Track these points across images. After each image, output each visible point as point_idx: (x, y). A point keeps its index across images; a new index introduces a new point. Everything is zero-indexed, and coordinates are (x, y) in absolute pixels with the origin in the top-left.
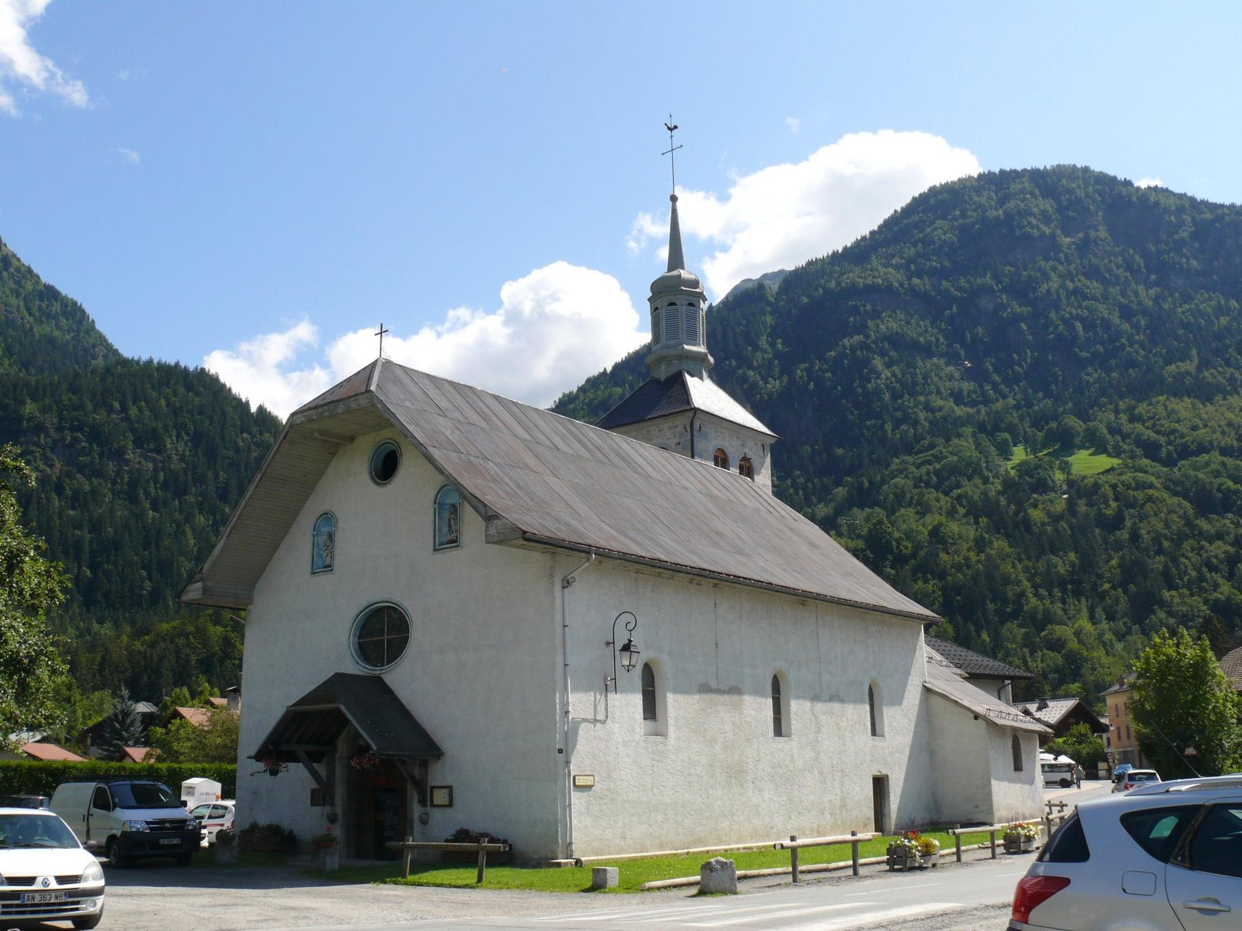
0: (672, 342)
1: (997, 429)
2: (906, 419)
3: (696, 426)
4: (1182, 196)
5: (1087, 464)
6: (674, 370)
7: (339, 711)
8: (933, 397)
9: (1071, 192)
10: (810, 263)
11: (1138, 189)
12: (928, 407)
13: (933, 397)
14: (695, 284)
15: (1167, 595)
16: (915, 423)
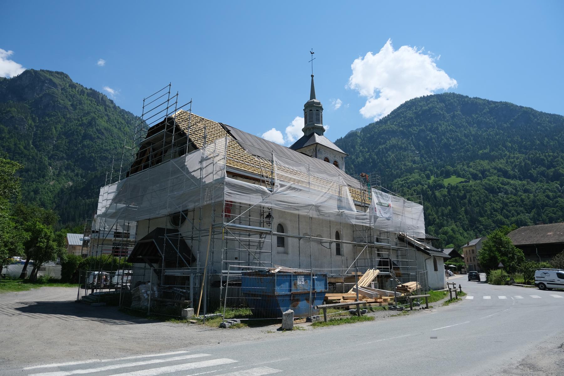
0: (311, 123)
1: (426, 170)
2: (398, 168)
3: (318, 149)
4: (484, 100)
5: (454, 180)
6: (311, 132)
7: (153, 242)
8: (406, 162)
9: (449, 100)
10: (370, 125)
11: (470, 98)
12: (405, 165)
13: (406, 162)
14: (319, 103)
15: (481, 219)
16: (401, 169)
